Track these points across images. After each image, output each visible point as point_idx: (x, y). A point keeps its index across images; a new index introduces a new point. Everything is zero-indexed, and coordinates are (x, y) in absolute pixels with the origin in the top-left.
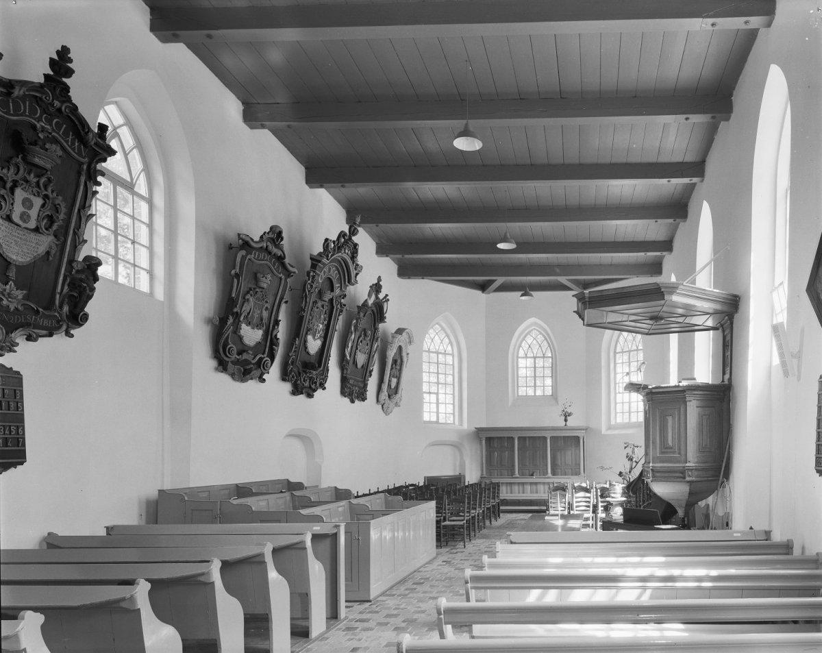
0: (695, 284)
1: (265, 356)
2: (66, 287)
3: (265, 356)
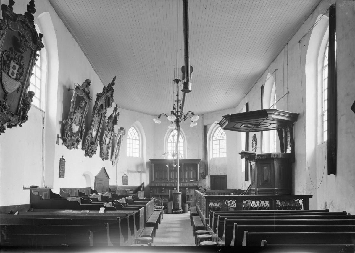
0: (184, 66)
1: (79, 137)
2: (22, 105)
3: (79, 137)
